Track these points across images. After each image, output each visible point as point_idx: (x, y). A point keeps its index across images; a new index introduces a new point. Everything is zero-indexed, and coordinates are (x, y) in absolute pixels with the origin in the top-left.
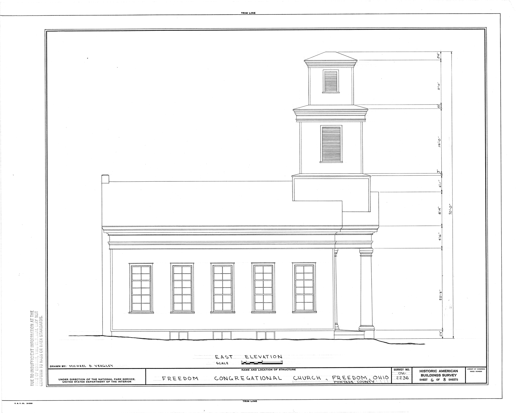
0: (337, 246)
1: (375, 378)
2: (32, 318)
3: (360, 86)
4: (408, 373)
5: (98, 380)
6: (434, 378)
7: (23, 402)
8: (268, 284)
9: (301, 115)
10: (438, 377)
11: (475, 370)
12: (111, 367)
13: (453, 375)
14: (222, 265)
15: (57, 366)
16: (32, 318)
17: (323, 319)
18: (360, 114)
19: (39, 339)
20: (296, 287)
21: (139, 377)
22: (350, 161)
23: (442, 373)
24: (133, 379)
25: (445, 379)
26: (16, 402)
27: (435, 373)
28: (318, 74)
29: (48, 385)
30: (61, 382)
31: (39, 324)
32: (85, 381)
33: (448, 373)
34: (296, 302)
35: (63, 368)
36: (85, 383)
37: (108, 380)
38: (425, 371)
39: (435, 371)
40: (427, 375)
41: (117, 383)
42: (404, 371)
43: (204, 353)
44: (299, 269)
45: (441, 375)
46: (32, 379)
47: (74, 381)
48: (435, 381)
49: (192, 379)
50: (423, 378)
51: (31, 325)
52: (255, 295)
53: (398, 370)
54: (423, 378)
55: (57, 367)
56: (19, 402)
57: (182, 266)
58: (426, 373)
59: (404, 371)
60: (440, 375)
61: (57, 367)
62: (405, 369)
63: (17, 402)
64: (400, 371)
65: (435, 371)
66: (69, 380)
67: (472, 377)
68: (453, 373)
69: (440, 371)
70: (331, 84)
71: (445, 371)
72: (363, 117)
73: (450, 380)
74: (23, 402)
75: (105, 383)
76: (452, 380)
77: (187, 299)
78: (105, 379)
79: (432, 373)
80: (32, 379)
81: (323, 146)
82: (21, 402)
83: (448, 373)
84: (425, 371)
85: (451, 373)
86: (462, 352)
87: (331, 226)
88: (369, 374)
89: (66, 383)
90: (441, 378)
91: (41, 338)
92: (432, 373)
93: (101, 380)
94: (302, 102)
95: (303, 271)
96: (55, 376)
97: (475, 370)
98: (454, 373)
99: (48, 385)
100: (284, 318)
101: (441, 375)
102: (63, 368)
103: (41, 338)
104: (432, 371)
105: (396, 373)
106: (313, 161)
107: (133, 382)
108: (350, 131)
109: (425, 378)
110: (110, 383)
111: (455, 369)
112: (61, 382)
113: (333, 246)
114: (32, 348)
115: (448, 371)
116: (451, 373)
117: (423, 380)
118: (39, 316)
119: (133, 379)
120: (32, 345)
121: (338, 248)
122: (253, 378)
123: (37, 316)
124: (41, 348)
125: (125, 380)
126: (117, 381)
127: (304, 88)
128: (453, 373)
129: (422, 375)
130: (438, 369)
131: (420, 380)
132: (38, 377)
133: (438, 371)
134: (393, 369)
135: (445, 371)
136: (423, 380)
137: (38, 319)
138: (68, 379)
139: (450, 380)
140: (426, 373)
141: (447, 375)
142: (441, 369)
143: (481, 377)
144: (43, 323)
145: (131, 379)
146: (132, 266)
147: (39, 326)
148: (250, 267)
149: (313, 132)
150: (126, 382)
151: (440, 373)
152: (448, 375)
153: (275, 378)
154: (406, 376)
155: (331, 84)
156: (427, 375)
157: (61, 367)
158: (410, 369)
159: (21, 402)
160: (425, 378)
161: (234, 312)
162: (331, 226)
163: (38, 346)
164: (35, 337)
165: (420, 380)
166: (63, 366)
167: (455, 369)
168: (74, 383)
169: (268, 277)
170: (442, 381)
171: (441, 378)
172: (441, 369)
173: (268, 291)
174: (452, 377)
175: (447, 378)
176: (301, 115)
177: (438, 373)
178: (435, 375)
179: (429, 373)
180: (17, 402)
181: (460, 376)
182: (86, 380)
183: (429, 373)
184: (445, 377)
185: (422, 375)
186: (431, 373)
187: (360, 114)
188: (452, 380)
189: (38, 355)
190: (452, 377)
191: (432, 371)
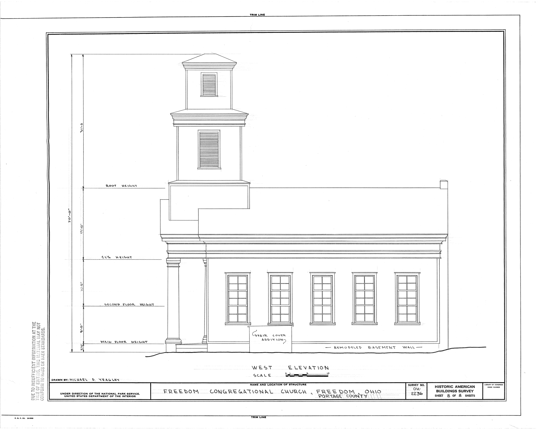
0: (208, 256)
1: (367, 392)
2: (34, 329)
3: (238, 91)
4: (423, 389)
5: (101, 395)
6: (451, 394)
7: (24, 417)
8: (285, 294)
9: (179, 120)
10: (454, 393)
11: (493, 386)
12: (117, 381)
13: (469, 391)
14: (238, 275)
15: (59, 380)
16: (34, 329)
17: (425, 331)
18: (240, 119)
19: (42, 351)
20: (229, 298)
21: (143, 391)
22: (229, 167)
23: (458, 389)
24: (138, 394)
25: (460, 395)
26: (17, 417)
27: (451, 389)
28: (195, 77)
29: (50, 399)
30: (63, 397)
31: (41, 336)
32: (88, 395)
33: (465, 389)
34: (271, 314)
35: (65, 381)
36: (88, 398)
37: (112, 394)
38: (440, 387)
39: (451, 387)
40: (442, 391)
41: (121, 398)
42: (419, 386)
43: (240, 369)
44: (233, 280)
45: (458, 391)
46: (33, 393)
47: (76, 395)
48: (451, 397)
49: (193, 392)
50: (439, 393)
51: (33, 337)
52: (313, 306)
53: (412, 385)
54: (439, 393)
55: (59, 381)
56: (19, 417)
57: (364, 276)
58: (441, 389)
59: (419, 386)
60: (456, 391)
61: (59, 381)
62: (419, 384)
63: (17, 417)
64: (415, 387)
65: (451, 387)
66: (71, 394)
67: (490, 393)
68: (469, 389)
69: (456, 387)
70: (209, 88)
71: (461, 387)
72: (243, 122)
73: (466, 396)
74: (24, 417)
75: (109, 398)
76: (469, 396)
77: (369, 310)
78: (109, 394)
79: (448, 389)
80: (33, 393)
81: (201, 153)
82: (22, 417)
83: (465, 389)
84: (440, 387)
85: (467, 389)
86: (480, 367)
87: (342, 235)
88: (359, 389)
89: (68, 397)
90: (458, 394)
91: (43, 350)
92: (448, 389)
93: (104, 395)
94: (179, 107)
95: (406, 282)
96: (57, 390)
97: (493, 386)
98: (471, 389)
99: (50, 399)
100: (344, 330)
101: (458, 391)
102: (65, 381)
103: (43, 350)
104: (448, 386)
105: (410, 389)
106: (190, 168)
107: (137, 397)
108: (228, 137)
109: (441, 393)
110: (114, 398)
111: (472, 384)
112: (63, 397)
113: (204, 256)
114: (33, 361)
115: (465, 386)
116: (467, 389)
117: (439, 396)
118: (42, 327)
119: (138, 394)
120: (33, 358)
121: (208, 258)
122: (245, 392)
123: (39, 328)
124: (43, 361)
125: (129, 395)
126: (121, 395)
127: (178, 90)
128: (469, 389)
129: (437, 391)
130: (454, 385)
131: (436, 396)
132: (40, 391)
133: (454, 386)
134: (407, 384)
135: (461, 387)
136: (439, 396)
137: (40, 331)
138: (70, 393)
139: (466, 396)
140: (441, 389)
141: (463, 390)
142: (457, 384)
143: (498, 393)
144: (43, 334)
145: (135, 394)
146: (228, 275)
147: (41, 338)
148: (351, 276)
149: (190, 136)
150: (131, 397)
151: (456, 389)
152: (465, 391)
153: (230, 392)
154: (420, 391)
155: (209, 88)
156: (442, 391)
157: (63, 381)
158: (425, 384)
159: (22, 417)
160: (441, 393)
161: (419, 323)
162: (342, 235)
163: (40, 359)
164: (37, 349)
165: (436, 396)
166: (65, 380)
167: (472, 384)
168: (76, 398)
169: (285, 287)
170: (457, 397)
171: (458, 394)
172: (457, 384)
173: (412, 302)
174: (468, 393)
175: (463, 394)
176: (179, 120)
177: (454, 389)
178: (451, 391)
179: (444, 389)
180: (17, 417)
181: (477, 392)
182: (88, 395)
183: (444, 389)
184: (461, 393)
185: (437, 391)
186: (446, 389)
187: (240, 119)
188: (469, 396)
189: (40, 368)
190: (468, 393)
191: (448, 386)
